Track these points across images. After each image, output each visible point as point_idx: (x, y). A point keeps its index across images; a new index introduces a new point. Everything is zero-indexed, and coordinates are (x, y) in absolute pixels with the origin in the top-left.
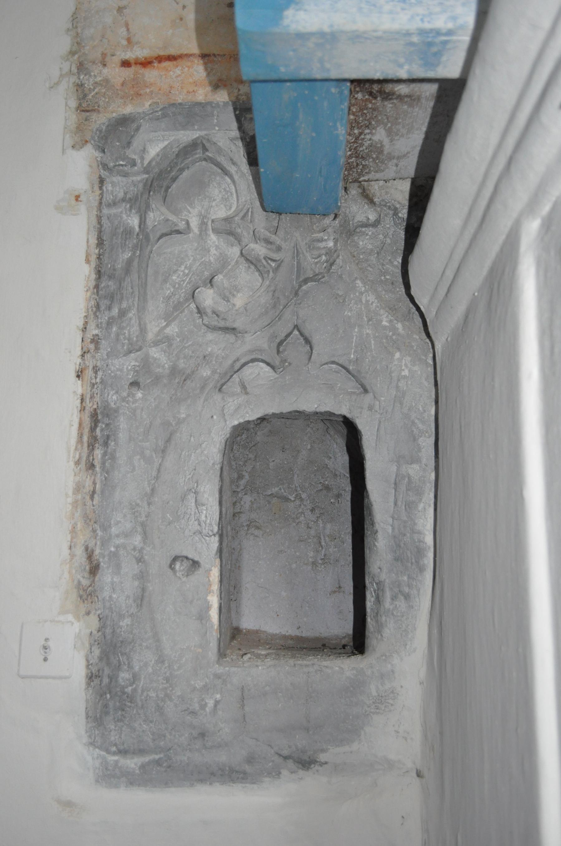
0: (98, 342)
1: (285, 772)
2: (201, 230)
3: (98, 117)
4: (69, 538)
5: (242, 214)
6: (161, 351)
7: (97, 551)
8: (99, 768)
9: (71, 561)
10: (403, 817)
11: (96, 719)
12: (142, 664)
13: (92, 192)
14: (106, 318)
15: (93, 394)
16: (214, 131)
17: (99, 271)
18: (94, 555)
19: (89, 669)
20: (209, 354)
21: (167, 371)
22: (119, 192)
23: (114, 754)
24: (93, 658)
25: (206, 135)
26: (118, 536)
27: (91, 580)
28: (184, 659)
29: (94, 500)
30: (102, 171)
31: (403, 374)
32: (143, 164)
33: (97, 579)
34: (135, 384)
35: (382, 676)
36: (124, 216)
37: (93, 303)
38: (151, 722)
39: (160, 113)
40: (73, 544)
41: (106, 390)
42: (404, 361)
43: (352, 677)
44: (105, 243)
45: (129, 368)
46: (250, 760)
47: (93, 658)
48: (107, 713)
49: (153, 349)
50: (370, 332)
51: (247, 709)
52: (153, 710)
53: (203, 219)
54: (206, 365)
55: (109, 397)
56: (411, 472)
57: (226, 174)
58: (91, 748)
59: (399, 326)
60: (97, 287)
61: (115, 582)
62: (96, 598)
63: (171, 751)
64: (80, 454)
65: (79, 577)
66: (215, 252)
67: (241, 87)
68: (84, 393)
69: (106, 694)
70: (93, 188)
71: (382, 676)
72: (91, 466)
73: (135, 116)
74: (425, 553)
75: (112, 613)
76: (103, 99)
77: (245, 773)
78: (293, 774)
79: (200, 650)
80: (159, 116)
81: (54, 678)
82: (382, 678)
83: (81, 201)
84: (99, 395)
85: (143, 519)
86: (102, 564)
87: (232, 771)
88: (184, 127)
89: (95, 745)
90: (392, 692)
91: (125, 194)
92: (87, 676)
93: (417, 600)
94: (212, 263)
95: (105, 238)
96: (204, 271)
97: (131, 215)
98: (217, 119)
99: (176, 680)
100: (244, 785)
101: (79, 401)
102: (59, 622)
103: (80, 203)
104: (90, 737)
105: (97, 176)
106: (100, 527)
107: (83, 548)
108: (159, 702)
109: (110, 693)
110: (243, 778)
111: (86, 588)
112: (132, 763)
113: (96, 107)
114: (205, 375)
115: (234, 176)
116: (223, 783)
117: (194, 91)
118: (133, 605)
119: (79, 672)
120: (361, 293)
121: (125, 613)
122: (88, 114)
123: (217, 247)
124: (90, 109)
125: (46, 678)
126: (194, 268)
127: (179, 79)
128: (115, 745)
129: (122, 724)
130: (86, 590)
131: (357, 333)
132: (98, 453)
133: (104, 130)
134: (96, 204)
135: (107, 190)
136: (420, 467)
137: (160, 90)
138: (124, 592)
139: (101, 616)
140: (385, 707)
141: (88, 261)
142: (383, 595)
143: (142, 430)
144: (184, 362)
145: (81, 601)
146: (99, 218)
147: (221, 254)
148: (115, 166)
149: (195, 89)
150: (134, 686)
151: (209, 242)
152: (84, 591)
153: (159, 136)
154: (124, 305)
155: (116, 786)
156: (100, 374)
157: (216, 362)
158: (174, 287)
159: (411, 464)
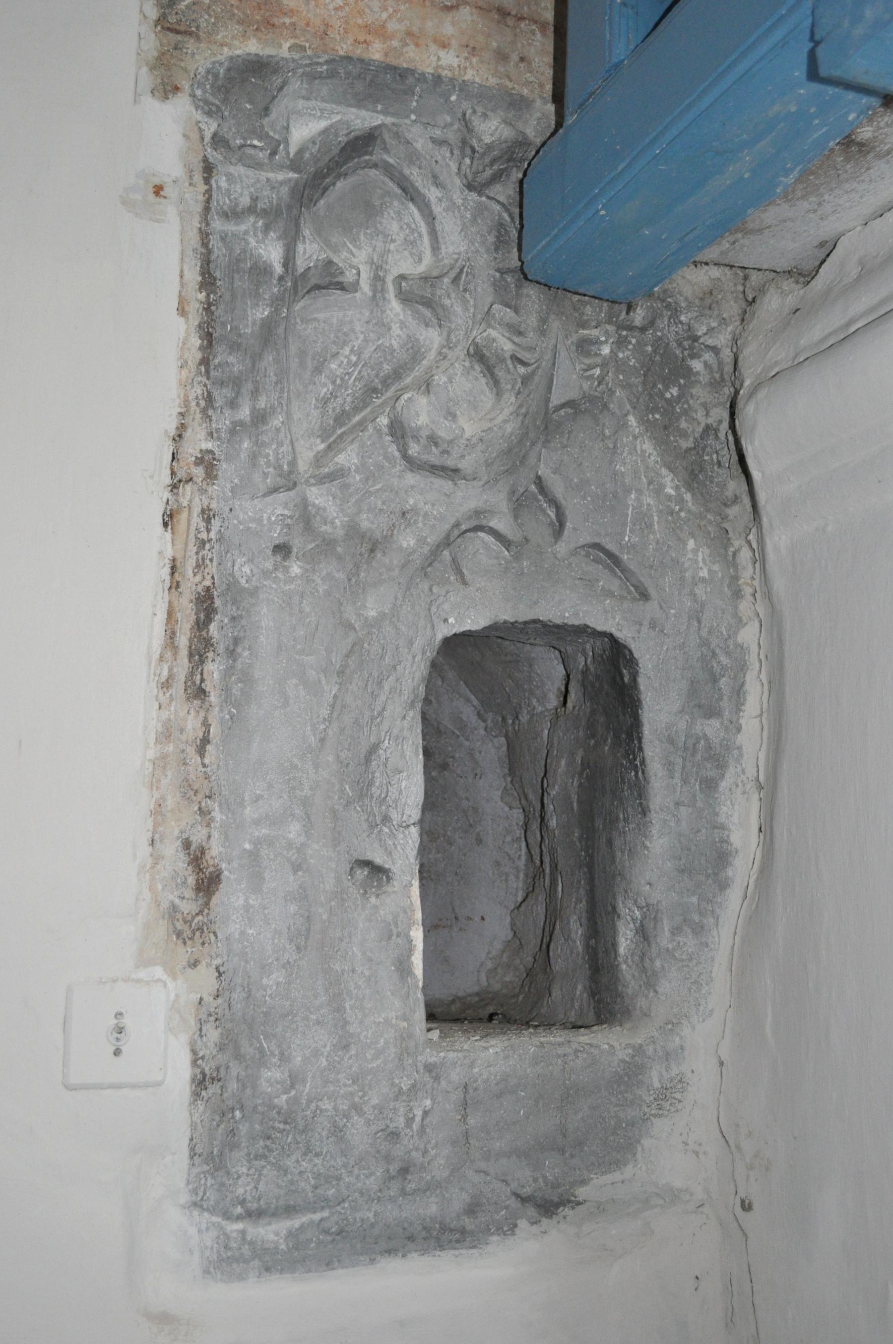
0: (213, 465)
1: (523, 1224)
2: (375, 291)
3: (198, 49)
4: (150, 824)
5: (453, 274)
6: (327, 495)
7: (215, 849)
8: (212, 1248)
9: (152, 867)
10: (697, 1278)
11: (209, 1158)
12: (308, 1052)
13: (190, 184)
14: (227, 422)
15: (203, 559)
16: (406, 121)
17: (210, 335)
18: (208, 857)
19: (199, 1067)
20: (412, 510)
21: (340, 533)
22: (241, 195)
23: (239, 1218)
24: (206, 1047)
25: (394, 124)
26: (257, 822)
27: (200, 902)
28: (382, 1041)
29: (207, 754)
30: (209, 150)
31: (701, 574)
32: (288, 153)
33: (215, 900)
34: (282, 550)
35: (668, 1055)
36: (252, 242)
37: (199, 392)
38: (317, 1155)
39: (325, 67)
40: (157, 836)
41: (229, 555)
42: (700, 554)
43: (627, 1059)
44: (219, 283)
45: (273, 519)
46: (472, 1210)
47: (206, 1047)
48: (234, 1146)
49: (313, 489)
50: (652, 503)
51: (471, 1121)
52: (324, 1134)
53: (377, 269)
54: (406, 528)
55: (236, 568)
56: (709, 732)
57: (412, 200)
58: (196, 1213)
59: (688, 497)
60: (205, 362)
61: (252, 907)
62: (212, 935)
63: (346, 1205)
64: (170, 669)
65: (171, 897)
66: (399, 332)
67: (442, 53)
68: (179, 557)
69: (233, 1110)
70: (191, 177)
71: (668, 1055)
72: (201, 693)
73: (278, 63)
74: (731, 859)
75: (246, 962)
76: (206, 17)
77: (463, 1231)
78: (535, 1226)
79: (405, 1024)
80: (322, 72)
81: (134, 1086)
82: (667, 1060)
83: (165, 197)
84: (215, 563)
85: (307, 791)
86: (226, 873)
87: (444, 1228)
88: (360, 102)
89: (201, 1206)
90: (680, 1081)
91: (254, 200)
92: (193, 1080)
93: (715, 933)
94: (395, 350)
95: (218, 274)
96: (381, 363)
97: (266, 242)
98: (417, 101)
99: (369, 1078)
100: (457, 1252)
101: (167, 570)
102: (138, 981)
103: (162, 200)
104: (195, 1192)
105: (200, 158)
106: (220, 805)
107: (179, 843)
108: (337, 1118)
109: (242, 1108)
110: (458, 1241)
111: (190, 918)
112: (272, 1232)
113: (194, 29)
114: (405, 546)
115: (433, 207)
116: (424, 1251)
117: (365, 41)
118: (288, 947)
119: (180, 1074)
120: (635, 438)
121: (272, 963)
122: (179, 37)
123: (403, 325)
124: (182, 28)
125: (101, 1087)
126: (366, 355)
127: (341, 14)
128: (243, 1202)
129: (263, 1163)
130: (191, 922)
131: (634, 501)
132: (214, 669)
133: (221, 75)
134: (199, 208)
135: (219, 188)
136: (722, 724)
137: (308, 24)
138: (269, 924)
139: (222, 969)
140: (671, 1105)
141: (182, 311)
142: (655, 928)
143: (302, 633)
144: (368, 519)
145: (180, 942)
146: (205, 236)
147: (409, 337)
148: (242, 146)
149: (369, 38)
150: (293, 1093)
151: (388, 312)
152: (185, 922)
153: (314, 109)
154: (262, 403)
155: (241, 1277)
156: (216, 523)
157: (425, 525)
158: (334, 382)
159: (709, 719)
